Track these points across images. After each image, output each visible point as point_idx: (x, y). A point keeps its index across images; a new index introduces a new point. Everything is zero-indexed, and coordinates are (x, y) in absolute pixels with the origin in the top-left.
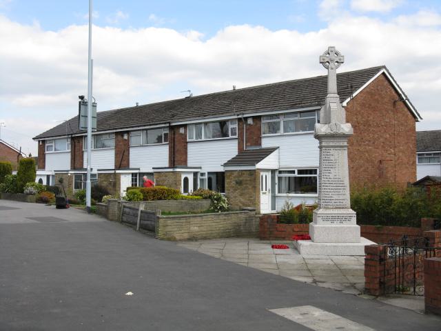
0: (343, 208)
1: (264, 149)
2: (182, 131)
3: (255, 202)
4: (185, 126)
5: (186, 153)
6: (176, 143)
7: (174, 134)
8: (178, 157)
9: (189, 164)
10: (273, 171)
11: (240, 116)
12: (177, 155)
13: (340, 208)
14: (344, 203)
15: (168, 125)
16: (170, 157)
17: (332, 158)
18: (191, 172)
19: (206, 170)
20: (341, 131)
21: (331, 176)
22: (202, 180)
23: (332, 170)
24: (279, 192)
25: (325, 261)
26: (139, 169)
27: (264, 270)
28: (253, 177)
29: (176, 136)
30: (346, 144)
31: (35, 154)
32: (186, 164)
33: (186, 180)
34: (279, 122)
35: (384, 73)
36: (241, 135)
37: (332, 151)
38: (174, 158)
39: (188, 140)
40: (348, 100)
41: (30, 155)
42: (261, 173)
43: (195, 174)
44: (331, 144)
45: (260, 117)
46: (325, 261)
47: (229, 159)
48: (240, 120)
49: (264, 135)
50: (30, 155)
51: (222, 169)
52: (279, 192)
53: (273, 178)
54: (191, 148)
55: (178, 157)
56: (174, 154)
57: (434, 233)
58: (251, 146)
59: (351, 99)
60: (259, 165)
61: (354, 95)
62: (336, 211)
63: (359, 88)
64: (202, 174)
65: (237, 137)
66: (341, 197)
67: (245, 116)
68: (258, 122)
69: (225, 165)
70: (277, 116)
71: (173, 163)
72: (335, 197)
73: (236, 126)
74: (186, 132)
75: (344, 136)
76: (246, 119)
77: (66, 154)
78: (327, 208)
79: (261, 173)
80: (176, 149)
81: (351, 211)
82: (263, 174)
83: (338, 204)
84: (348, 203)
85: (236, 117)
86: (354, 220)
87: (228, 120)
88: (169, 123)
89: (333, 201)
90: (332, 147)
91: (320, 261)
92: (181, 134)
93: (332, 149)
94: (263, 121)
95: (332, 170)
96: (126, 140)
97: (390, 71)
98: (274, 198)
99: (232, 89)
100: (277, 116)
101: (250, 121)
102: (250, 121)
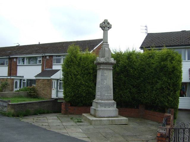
1: (54, 70)
2: (15, 60)
3: (51, 94)
4: (17, 58)
5: (16, 71)
6: (12, 65)
9: (18, 75)
10: (58, 80)
11: (43, 55)
15: (8, 57)
19: (26, 78)
20: (110, 62)
21: (105, 84)
22: (24, 83)
23: (105, 81)
24: (59, 89)
27: (79, 138)
28: (49, 82)
30: (112, 68)
31: (17, 75)
32: (16, 75)
33: (16, 82)
34: (61, 59)
36: (43, 64)
37: (105, 71)
38: (10, 72)
39: (18, 64)
40: (92, 51)
41: (39, 43)
42: (53, 80)
43: (21, 80)
44: (105, 68)
45: (52, 56)
47: (36, 75)
48: (43, 56)
49: (53, 64)
50: (39, 43)
51: (34, 78)
52: (59, 89)
53: (57, 83)
54: (19, 68)
55: (12, 71)
56: (11, 70)
58: (48, 68)
60: (52, 77)
61: (94, 49)
62: (106, 102)
63: (96, 46)
64: (24, 80)
65: (41, 64)
67: (45, 55)
69: (36, 76)
70: (59, 56)
71: (10, 74)
72: (106, 94)
73: (41, 59)
74: (17, 61)
75: (111, 64)
76: (46, 56)
77: (60, 65)
79: (53, 80)
80: (12, 68)
81: (113, 101)
82: (53, 81)
84: (112, 97)
85: (41, 55)
86: (115, 106)
87: (37, 57)
88: (9, 56)
89: (105, 96)
90: (106, 69)
91: (23, 100)
94: (54, 58)
95: (105, 81)
96: (15, 62)
98: (57, 91)
99: (38, 44)
100: (59, 56)
101: (48, 57)
102: (48, 57)
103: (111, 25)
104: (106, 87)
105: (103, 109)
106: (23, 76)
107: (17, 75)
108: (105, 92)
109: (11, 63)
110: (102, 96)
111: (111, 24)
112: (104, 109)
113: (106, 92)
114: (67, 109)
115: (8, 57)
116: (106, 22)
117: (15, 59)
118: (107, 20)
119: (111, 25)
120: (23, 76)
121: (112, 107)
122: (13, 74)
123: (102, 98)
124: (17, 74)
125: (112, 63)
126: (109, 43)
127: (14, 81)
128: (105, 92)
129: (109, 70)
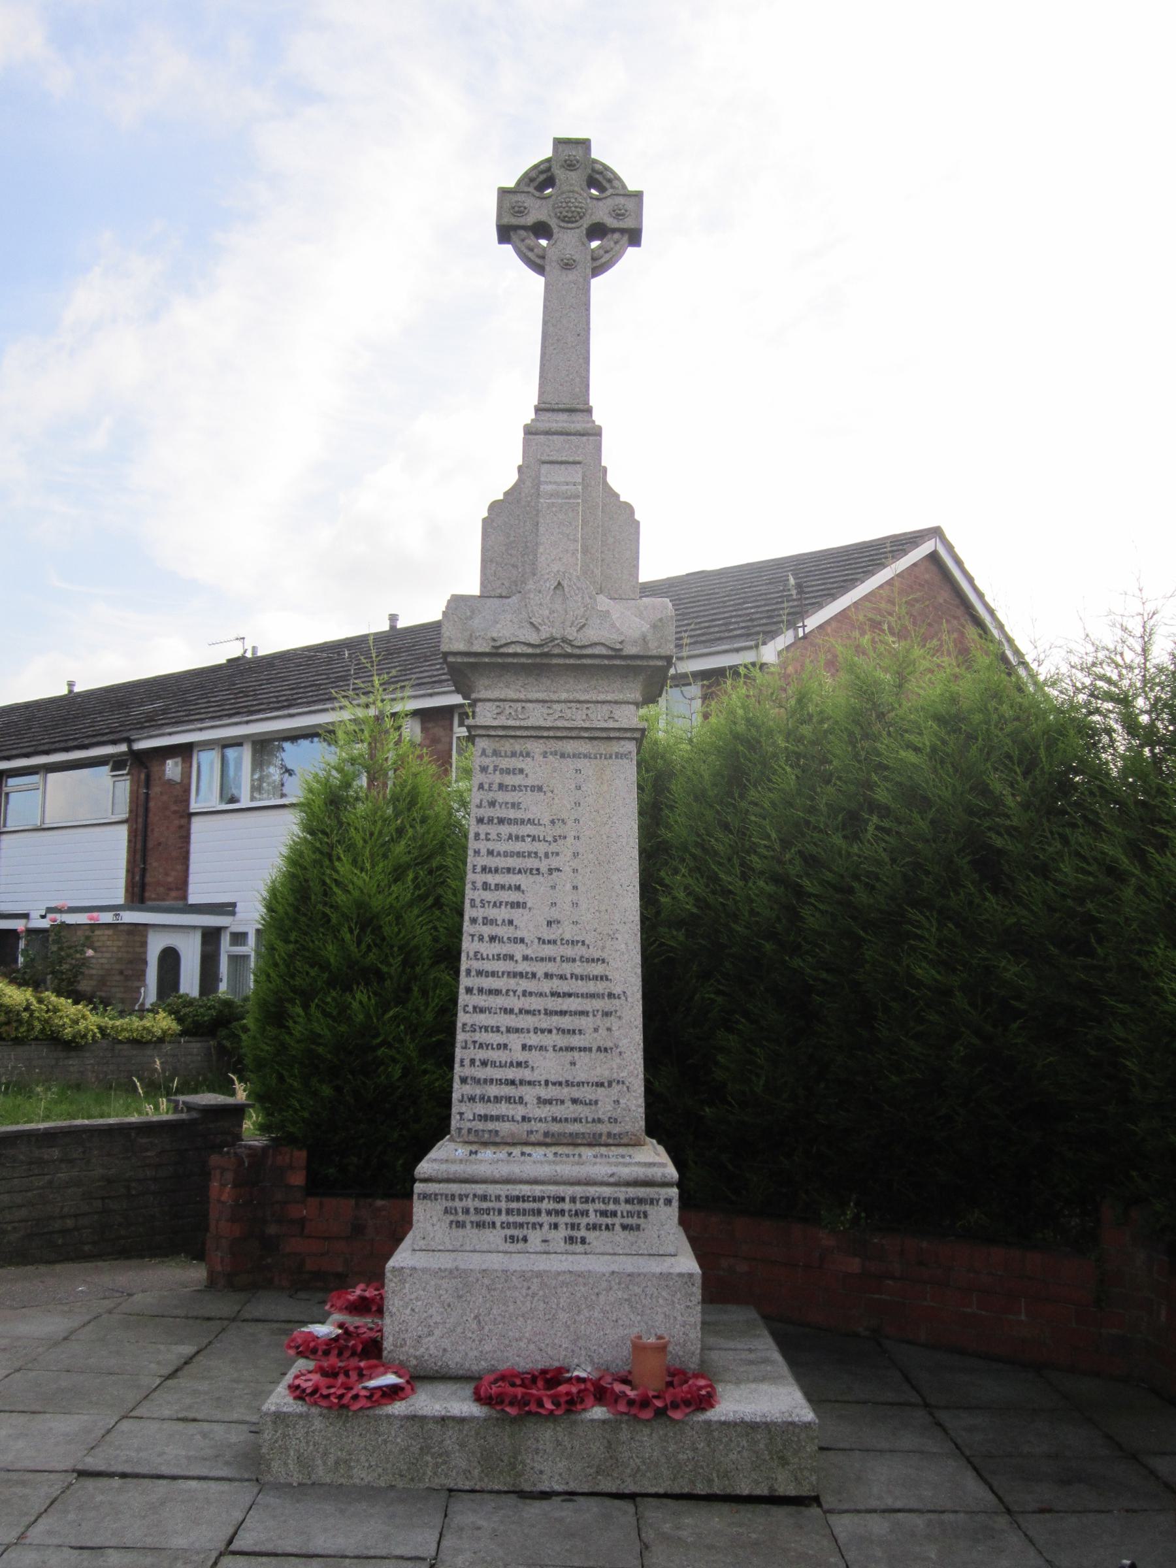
0: (594, 1142)
2: (172, 769)
4: (185, 751)
6: (153, 818)
7: (148, 783)
8: (156, 871)
12: (153, 863)
13: (573, 1141)
14: (605, 1109)
15: (123, 748)
16: (130, 871)
17: (535, 806)
18: (194, 927)
23: (535, 890)
25: (739, 1346)
26: (26, 916)
29: (156, 790)
31: (193, 899)
32: (185, 897)
33: (170, 958)
35: (934, 557)
37: (537, 768)
38: (144, 871)
40: (784, 640)
43: (211, 937)
46: (739, 1346)
57: (1167, 837)
59: (797, 639)
61: (813, 622)
64: (239, 938)
66: (588, 1068)
68: (439, 731)
72: (548, 1066)
74: (187, 774)
78: (481, 1141)
83: (568, 1110)
88: (129, 741)
89: (529, 1093)
92: (170, 782)
93: (536, 747)
95: (535, 890)
97: (958, 550)
99: (385, 627)
103: (638, 195)
104: (540, 969)
105: (475, 1262)
106: (234, 905)
107: (193, 899)
108: (533, 1039)
109: (147, 794)
110: (493, 1091)
111: (632, 187)
112: (495, 1262)
113: (548, 1040)
114: (272, 1230)
115: (123, 748)
116: (570, 165)
117: (170, 762)
118: (585, 144)
119: (638, 195)
120: (234, 905)
121: (620, 1236)
122: (161, 890)
123: (481, 1109)
124: (192, 888)
125: (617, 654)
126: (598, 417)
127: (144, 944)
128: (533, 1039)
129: (584, 747)
